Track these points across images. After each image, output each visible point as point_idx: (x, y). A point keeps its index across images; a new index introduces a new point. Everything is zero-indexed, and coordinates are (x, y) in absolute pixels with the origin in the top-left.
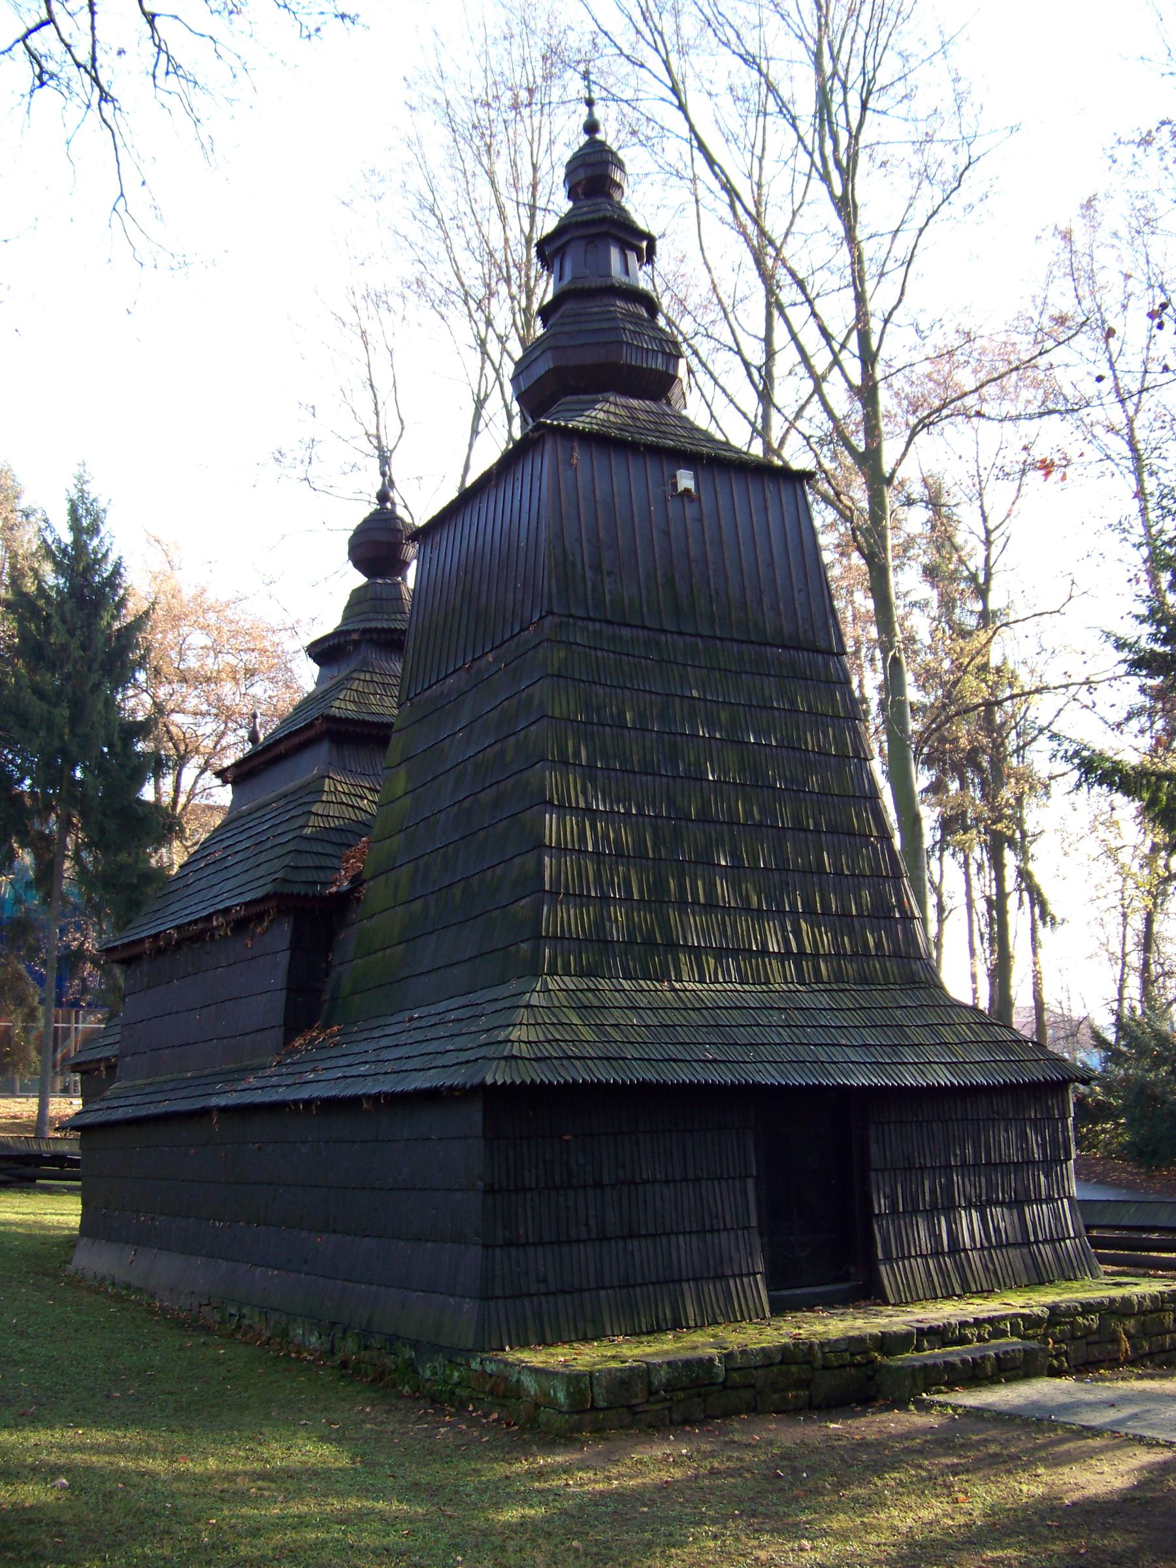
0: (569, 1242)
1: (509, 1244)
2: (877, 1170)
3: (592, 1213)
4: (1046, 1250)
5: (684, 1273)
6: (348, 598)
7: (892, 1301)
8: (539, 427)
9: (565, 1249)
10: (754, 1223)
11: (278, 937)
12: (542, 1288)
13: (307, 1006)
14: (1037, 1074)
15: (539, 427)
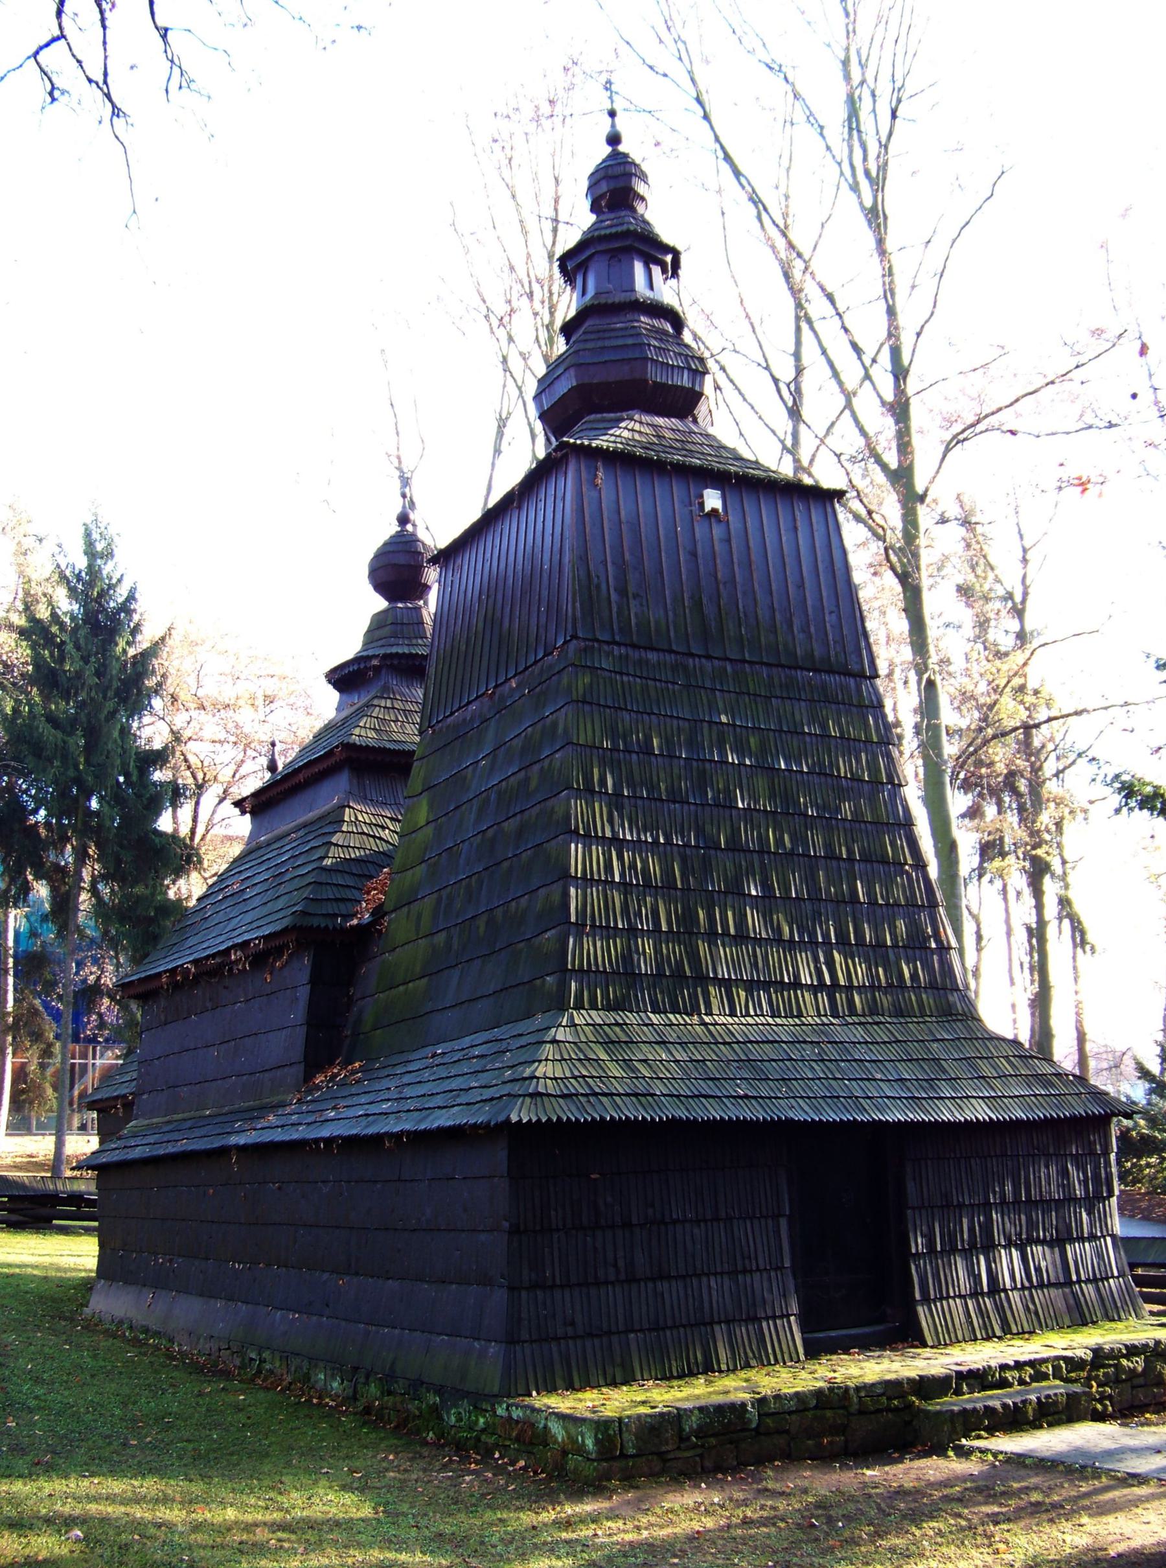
3: (621, 1254)
14: (1079, 1108)
15: (562, 446)
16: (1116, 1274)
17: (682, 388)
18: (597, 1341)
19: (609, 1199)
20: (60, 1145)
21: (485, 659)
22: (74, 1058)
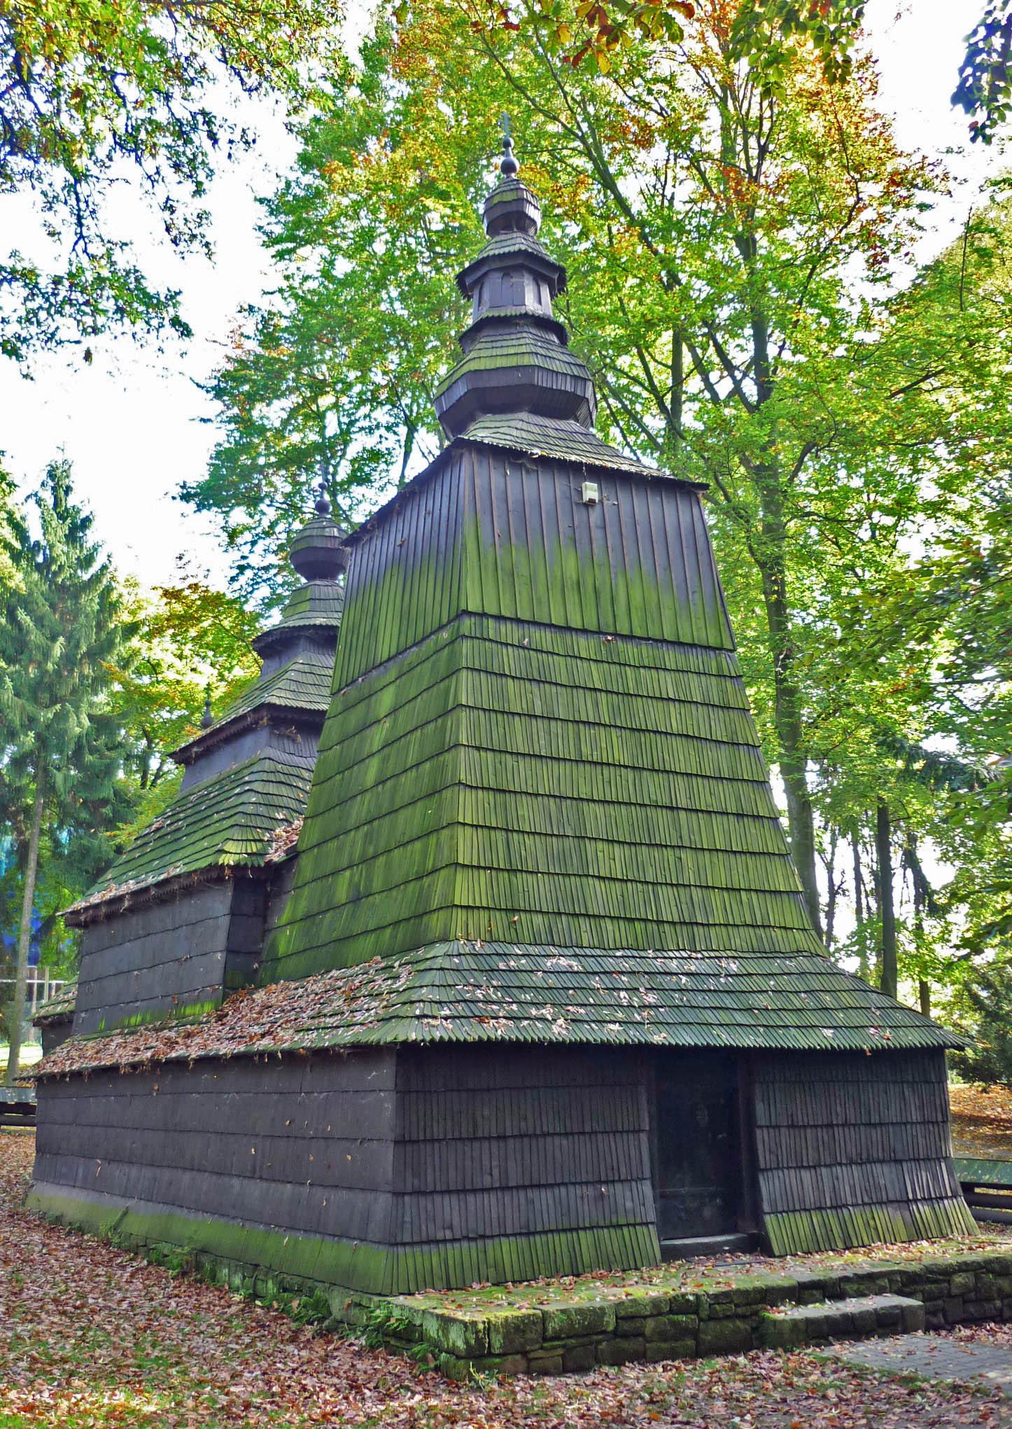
0: (474, 1191)
1: (418, 1193)
2: (761, 1127)
3: (495, 1163)
4: (925, 1209)
5: (603, 1174)
6: (928, 879)
7: (777, 1253)
8: (460, 444)
9: (471, 1198)
10: (647, 1174)
11: (219, 904)
12: (449, 1235)
13: (247, 968)
14: (913, 1038)
15: (460, 444)
16: (949, 1194)
17: (566, 392)
18: (473, 1244)
19: (486, 1113)
20: (14, 1055)
21: (388, 632)
22: (31, 977)
